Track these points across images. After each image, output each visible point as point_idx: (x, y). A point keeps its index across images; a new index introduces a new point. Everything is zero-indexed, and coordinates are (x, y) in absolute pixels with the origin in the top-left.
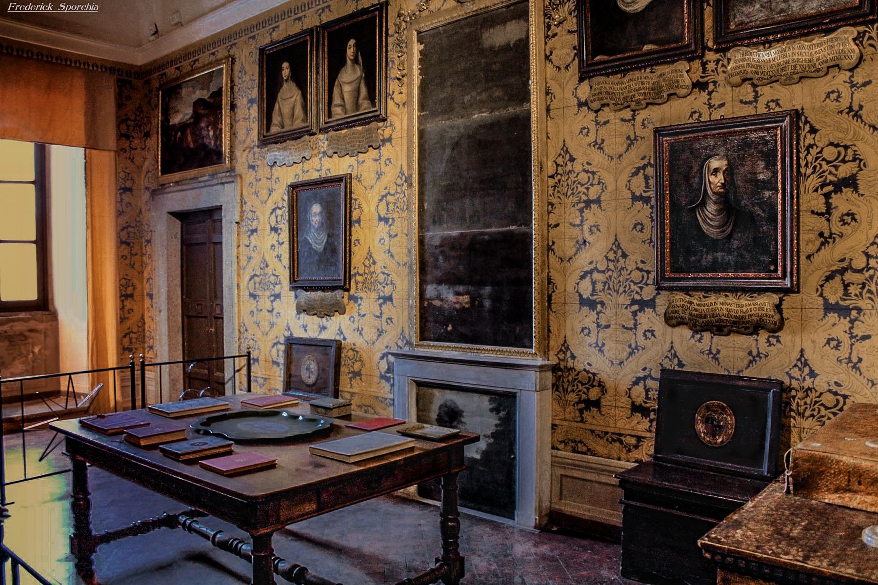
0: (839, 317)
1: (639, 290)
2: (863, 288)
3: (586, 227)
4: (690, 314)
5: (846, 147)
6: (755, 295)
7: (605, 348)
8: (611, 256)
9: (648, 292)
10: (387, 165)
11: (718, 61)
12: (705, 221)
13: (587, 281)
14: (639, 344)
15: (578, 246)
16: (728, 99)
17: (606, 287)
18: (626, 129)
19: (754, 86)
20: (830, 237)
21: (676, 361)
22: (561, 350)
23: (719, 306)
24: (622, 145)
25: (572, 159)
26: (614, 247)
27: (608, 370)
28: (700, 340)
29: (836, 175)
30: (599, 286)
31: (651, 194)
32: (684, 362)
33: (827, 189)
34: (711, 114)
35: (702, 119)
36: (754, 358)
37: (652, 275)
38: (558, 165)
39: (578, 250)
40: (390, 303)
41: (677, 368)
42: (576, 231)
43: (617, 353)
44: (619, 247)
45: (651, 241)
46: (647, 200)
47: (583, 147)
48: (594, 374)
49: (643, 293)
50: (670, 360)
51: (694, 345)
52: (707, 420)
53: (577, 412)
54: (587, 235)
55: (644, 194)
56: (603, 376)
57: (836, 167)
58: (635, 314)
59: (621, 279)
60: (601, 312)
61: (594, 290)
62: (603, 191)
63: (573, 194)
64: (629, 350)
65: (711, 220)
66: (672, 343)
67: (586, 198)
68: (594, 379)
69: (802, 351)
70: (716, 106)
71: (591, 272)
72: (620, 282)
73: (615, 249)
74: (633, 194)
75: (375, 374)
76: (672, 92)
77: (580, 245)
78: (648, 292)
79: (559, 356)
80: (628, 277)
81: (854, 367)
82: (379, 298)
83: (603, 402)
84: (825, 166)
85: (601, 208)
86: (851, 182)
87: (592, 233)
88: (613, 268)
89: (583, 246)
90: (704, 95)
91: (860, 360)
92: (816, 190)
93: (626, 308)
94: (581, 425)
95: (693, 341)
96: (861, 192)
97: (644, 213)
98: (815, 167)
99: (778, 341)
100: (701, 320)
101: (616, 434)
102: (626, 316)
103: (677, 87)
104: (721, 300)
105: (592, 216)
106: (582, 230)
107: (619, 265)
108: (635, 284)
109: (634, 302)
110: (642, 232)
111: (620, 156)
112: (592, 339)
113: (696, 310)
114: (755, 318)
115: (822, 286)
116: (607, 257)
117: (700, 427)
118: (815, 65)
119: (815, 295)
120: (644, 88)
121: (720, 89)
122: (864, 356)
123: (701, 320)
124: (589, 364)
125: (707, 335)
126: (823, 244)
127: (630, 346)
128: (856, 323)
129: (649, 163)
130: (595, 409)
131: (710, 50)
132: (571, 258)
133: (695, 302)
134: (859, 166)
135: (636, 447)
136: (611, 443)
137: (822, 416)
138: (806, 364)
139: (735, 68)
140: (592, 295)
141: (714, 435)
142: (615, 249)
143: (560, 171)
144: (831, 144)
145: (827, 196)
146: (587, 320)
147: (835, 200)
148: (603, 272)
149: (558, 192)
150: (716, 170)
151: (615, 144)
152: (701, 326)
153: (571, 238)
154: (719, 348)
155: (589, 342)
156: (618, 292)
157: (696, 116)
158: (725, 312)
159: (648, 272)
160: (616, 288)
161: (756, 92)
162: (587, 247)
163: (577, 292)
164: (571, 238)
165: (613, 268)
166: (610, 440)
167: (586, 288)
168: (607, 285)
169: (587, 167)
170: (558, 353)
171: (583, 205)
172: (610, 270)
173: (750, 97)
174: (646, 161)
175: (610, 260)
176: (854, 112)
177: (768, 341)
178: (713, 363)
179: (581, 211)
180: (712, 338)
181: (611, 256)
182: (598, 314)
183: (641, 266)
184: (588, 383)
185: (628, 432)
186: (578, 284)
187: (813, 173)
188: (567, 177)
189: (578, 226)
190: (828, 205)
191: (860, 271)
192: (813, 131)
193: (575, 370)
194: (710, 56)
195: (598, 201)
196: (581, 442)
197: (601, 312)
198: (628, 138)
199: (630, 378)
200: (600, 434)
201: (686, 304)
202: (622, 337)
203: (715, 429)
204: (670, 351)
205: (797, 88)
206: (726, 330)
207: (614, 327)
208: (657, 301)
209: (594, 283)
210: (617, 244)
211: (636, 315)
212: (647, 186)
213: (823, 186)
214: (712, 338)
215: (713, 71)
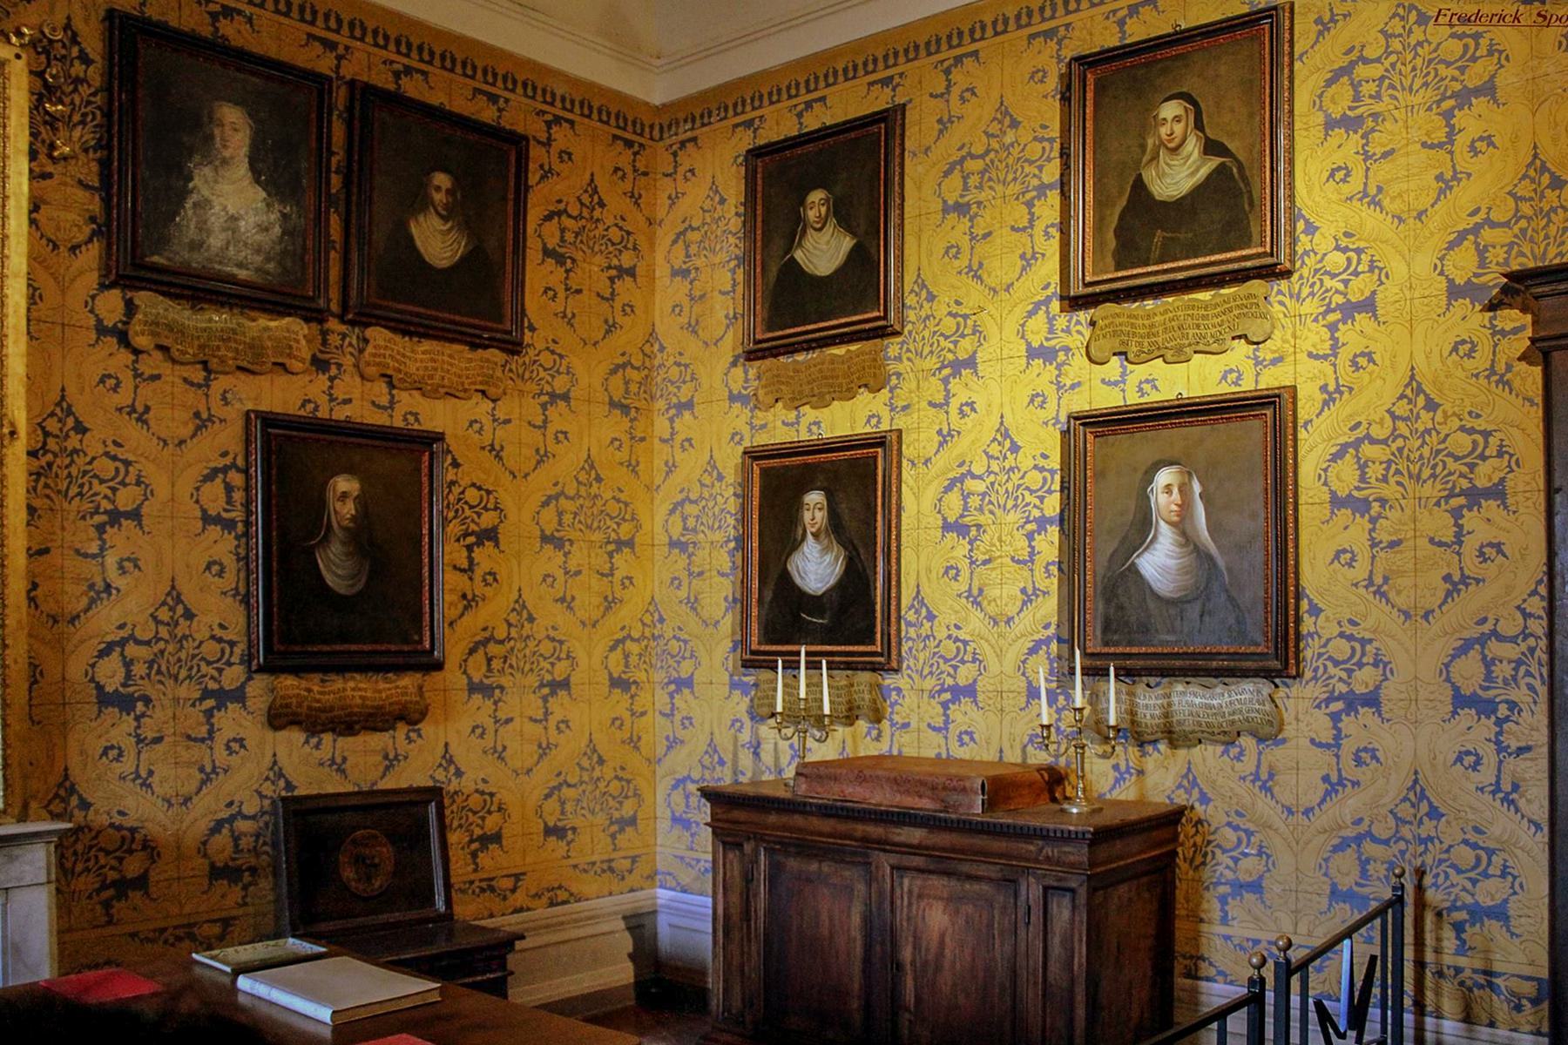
0: (121, 712)
1: (216, 674)
2: (505, 662)
3: (111, 560)
4: (310, 708)
5: (489, 492)
6: (390, 675)
7: (155, 780)
8: (164, 615)
9: (233, 676)
10: (558, 442)
11: (344, 335)
12: (329, 569)
13: (479, 656)
14: (217, 764)
15: (92, 594)
16: (356, 395)
17: (153, 672)
18: (193, 398)
19: (391, 386)
20: (473, 600)
21: (282, 783)
22: (57, 795)
23: (349, 693)
24: (186, 424)
25: (81, 429)
26: (169, 599)
27: (161, 816)
28: (317, 746)
29: (477, 524)
30: (139, 669)
31: (237, 514)
32: (295, 783)
33: (470, 540)
34: (331, 410)
35: (319, 415)
36: (391, 761)
37: (238, 650)
38: (46, 434)
39: (92, 602)
40: (237, 706)
41: (284, 793)
42: (90, 569)
43: (179, 784)
44: (178, 600)
45: (238, 593)
46: (229, 525)
47: (106, 411)
48: (133, 830)
49: (223, 678)
50: (273, 783)
51: (310, 754)
52: (359, 860)
53: (98, 907)
54: (113, 575)
55: (225, 515)
56: (152, 829)
57: (479, 515)
58: (209, 714)
59: (183, 655)
60: (143, 715)
61: (128, 675)
62: (147, 499)
63: (80, 494)
64: (199, 776)
65: (338, 567)
66: (275, 755)
67: (110, 507)
68: (133, 839)
69: (446, 745)
70: (146, 376)
71: (122, 643)
72: (180, 660)
73: (171, 603)
74: (204, 511)
75: (534, 830)
76: (280, 360)
77: (98, 593)
78: (233, 676)
79: (51, 807)
80: (196, 652)
81: (499, 757)
82: (542, 685)
83: (154, 876)
84: (468, 512)
85: (141, 528)
86: (490, 535)
87: (124, 573)
88: (167, 637)
89: (104, 595)
90: (323, 379)
91: (151, 773)
92: (458, 540)
93: (193, 705)
94: (110, 930)
95: (307, 749)
96: (502, 548)
97: (223, 546)
98: (457, 511)
99: (420, 736)
100: (323, 716)
101: (183, 926)
102: (193, 720)
103: (290, 356)
104: (351, 684)
105: (121, 540)
106: (102, 564)
107: (179, 632)
108: (209, 663)
109: (206, 694)
110: (220, 576)
111: (182, 442)
112: (127, 765)
113: (318, 701)
114: (396, 707)
115: (465, 661)
116: (154, 618)
117: (349, 874)
118: (463, 384)
119: (458, 673)
120: (235, 341)
121: (347, 378)
122: (507, 743)
123: (323, 716)
124: (121, 813)
125: (327, 738)
126: (466, 608)
127: (202, 770)
128: (500, 704)
129: (234, 465)
130: (139, 894)
131: (333, 315)
132: (78, 616)
133: (316, 688)
134: (145, 495)
135: (513, 890)
136: (173, 945)
137: (103, 867)
138: (451, 761)
139: (375, 355)
140: (124, 685)
141: (369, 879)
142: (171, 603)
143: (583, 491)
144: (473, 485)
145: (470, 548)
146: (114, 732)
147: (478, 553)
148: (148, 643)
149: (46, 486)
150: (344, 495)
151: (172, 420)
152: (323, 725)
153: (78, 580)
154: (346, 754)
155: (118, 771)
156: (176, 679)
157: (310, 407)
158: (359, 701)
159: (232, 644)
160: (174, 670)
161: (393, 396)
162: (113, 597)
163: (92, 680)
164: (78, 580)
165: (167, 637)
166: (171, 940)
167: (111, 673)
168: (156, 666)
169: (112, 449)
170: (50, 802)
171: (104, 518)
172: (162, 639)
173: (384, 401)
174: (228, 461)
175: (162, 622)
176: (496, 452)
177: (408, 737)
178: (143, 793)
179: (101, 529)
180: (335, 741)
181: (164, 615)
182: (137, 719)
183: (218, 632)
184: (121, 847)
185: (205, 917)
186: (93, 666)
187: (455, 517)
188: (67, 461)
189: (94, 556)
190: (471, 560)
191: (501, 642)
192: (456, 464)
193: (90, 830)
194: (333, 324)
195: (135, 515)
196: (560, 887)
197: (143, 715)
198: (197, 415)
199: (204, 825)
200: (151, 935)
201: (302, 693)
202: (185, 755)
203: (367, 867)
204: (271, 769)
205: (439, 404)
206: (357, 727)
207: (171, 739)
208: (248, 689)
209: (128, 664)
210: (175, 596)
211: (212, 716)
212: (229, 501)
213: (466, 535)
214: (335, 741)
215: (336, 347)
